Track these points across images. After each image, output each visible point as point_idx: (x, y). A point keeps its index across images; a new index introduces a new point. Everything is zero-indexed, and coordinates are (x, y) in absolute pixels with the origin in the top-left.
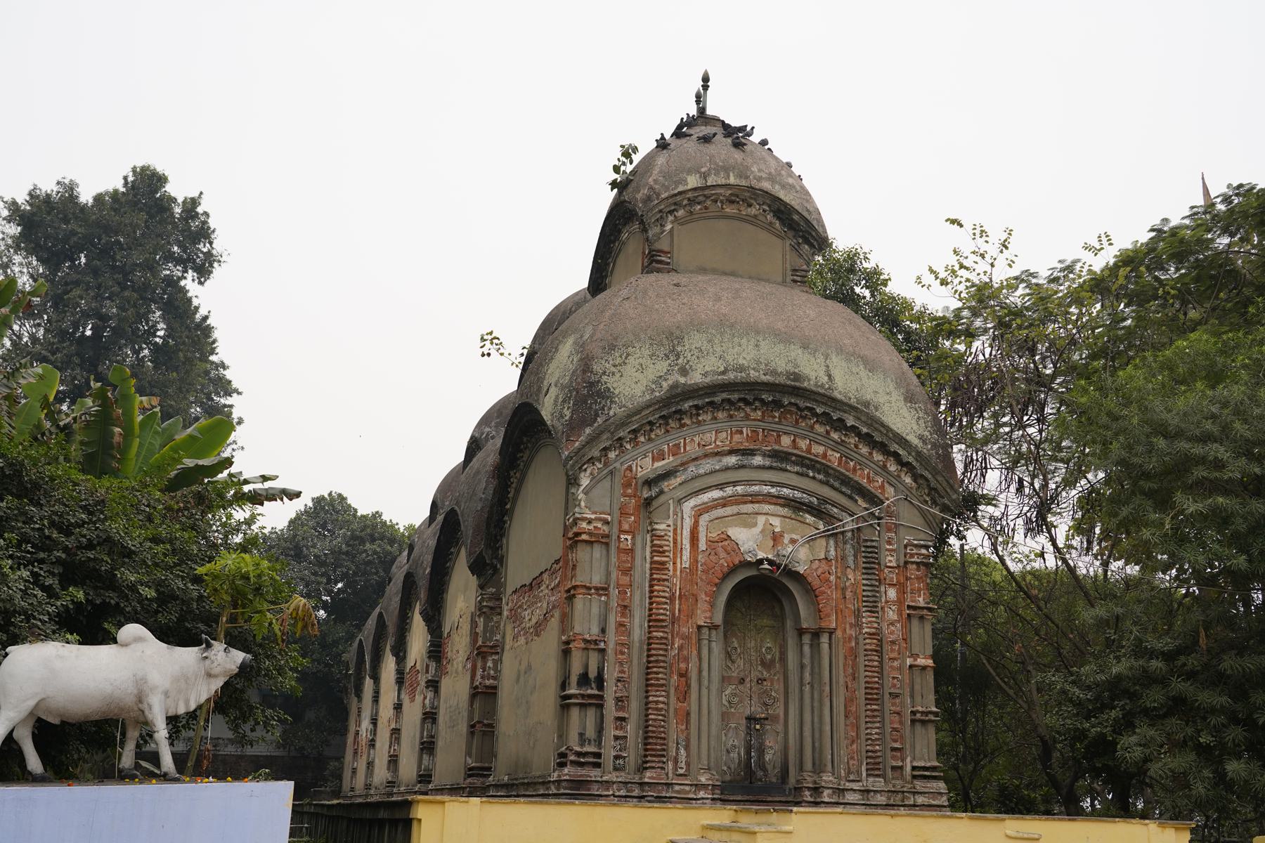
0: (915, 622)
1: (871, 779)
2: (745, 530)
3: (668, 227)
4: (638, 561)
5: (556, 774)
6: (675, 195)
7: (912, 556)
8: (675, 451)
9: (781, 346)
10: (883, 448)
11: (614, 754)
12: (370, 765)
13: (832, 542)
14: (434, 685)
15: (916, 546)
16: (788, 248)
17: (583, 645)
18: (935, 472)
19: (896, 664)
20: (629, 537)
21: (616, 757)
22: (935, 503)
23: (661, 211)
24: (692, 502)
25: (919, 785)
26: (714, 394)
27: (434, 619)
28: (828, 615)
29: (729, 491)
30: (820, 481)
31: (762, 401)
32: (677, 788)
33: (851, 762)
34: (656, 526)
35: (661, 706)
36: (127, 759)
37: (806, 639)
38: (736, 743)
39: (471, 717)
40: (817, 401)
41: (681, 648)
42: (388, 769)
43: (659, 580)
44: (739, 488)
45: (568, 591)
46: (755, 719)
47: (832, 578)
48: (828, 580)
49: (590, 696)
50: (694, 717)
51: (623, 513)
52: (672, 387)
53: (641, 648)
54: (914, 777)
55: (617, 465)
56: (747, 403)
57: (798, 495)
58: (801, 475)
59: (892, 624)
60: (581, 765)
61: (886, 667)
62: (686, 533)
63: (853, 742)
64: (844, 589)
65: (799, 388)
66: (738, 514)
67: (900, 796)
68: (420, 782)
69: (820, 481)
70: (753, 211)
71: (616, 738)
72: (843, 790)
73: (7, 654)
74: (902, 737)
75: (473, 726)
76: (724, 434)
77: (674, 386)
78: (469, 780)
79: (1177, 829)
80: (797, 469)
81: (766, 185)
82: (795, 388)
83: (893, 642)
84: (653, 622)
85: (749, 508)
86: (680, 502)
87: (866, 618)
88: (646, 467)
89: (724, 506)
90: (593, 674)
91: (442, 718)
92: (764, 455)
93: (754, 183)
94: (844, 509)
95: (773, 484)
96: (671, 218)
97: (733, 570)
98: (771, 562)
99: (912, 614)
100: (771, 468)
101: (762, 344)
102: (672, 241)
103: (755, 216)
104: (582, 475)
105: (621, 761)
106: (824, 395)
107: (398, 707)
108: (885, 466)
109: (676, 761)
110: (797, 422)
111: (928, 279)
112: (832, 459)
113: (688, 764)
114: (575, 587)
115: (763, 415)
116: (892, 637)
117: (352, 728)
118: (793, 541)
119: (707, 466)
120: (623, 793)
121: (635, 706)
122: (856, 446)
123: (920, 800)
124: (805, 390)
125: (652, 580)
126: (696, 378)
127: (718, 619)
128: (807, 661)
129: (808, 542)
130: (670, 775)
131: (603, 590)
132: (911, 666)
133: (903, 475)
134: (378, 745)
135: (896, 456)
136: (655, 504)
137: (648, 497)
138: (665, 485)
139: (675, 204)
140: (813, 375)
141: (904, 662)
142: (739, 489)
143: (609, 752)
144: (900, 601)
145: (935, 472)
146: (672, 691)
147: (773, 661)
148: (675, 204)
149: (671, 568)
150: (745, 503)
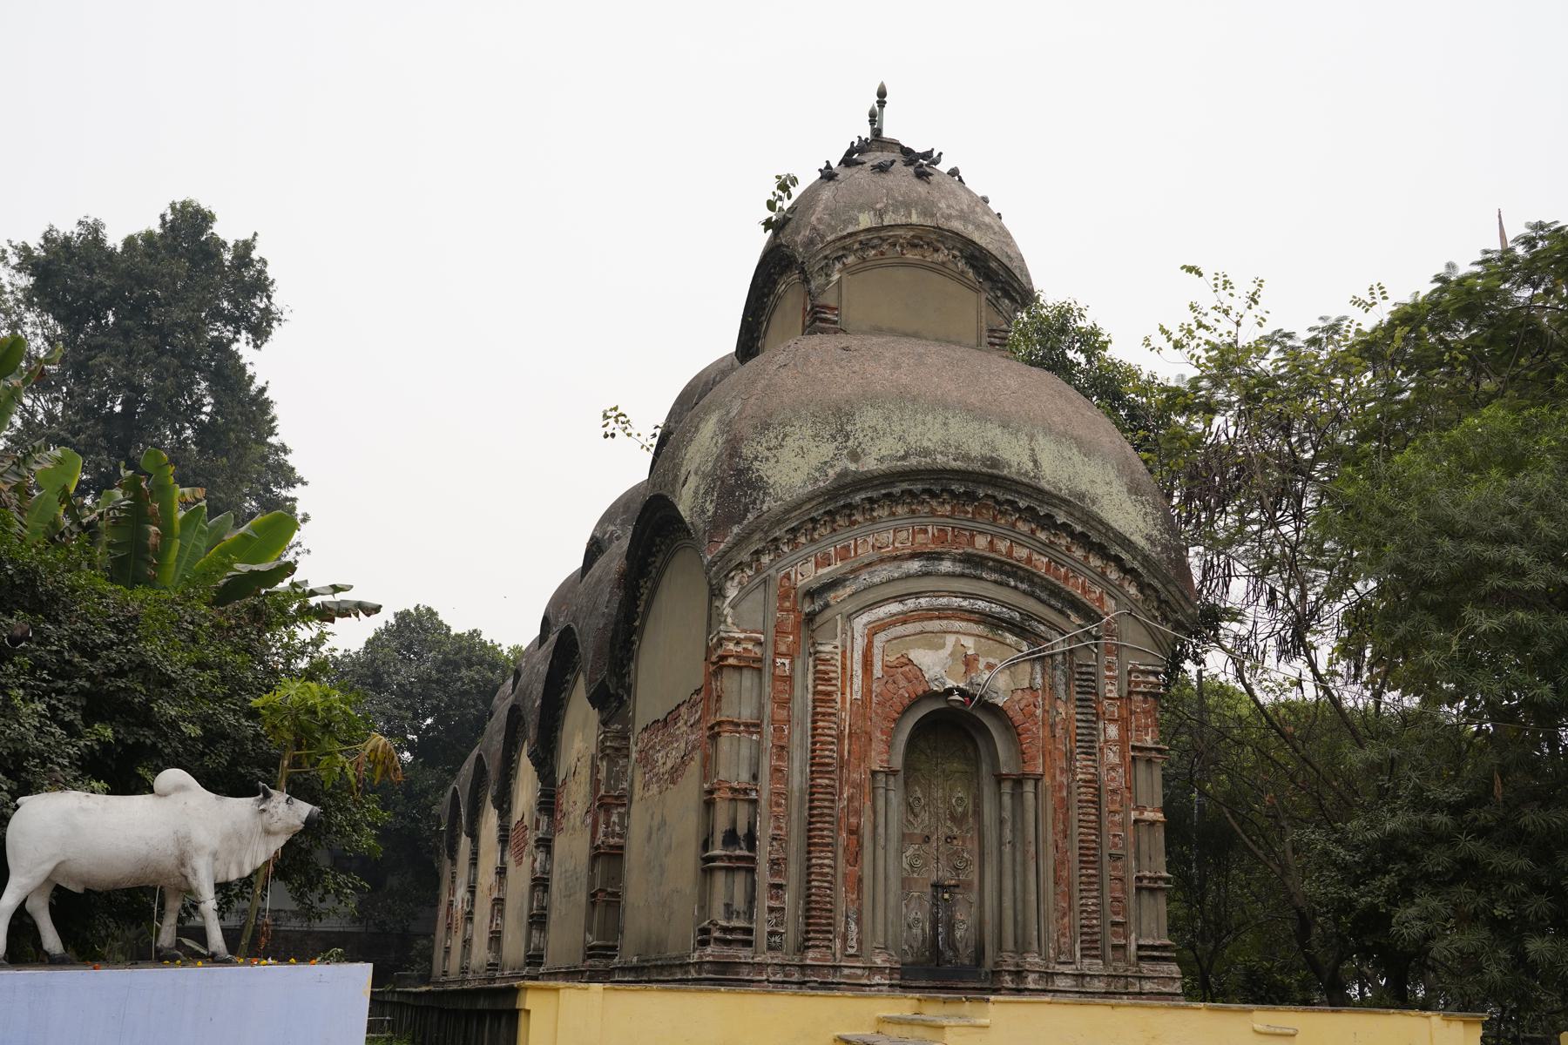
0: (1141, 767)
1: (1087, 961)
2: (930, 652)
3: (836, 277)
4: (798, 692)
5: (696, 955)
6: (844, 237)
7: (1137, 684)
8: (844, 554)
9: (976, 425)
10: (1101, 551)
12: (467, 943)
13: (1038, 668)
14: (545, 844)
15: (1142, 672)
17: (730, 795)
18: (1166, 581)
19: (1117, 818)
20: (787, 662)
21: (771, 934)
22: (1165, 618)
23: (826, 257)
24: (866, 618)
25: (1146, 968)
26: (892, 484)
27: (545, 763)
28: (1034, 758)
29: (911, 603)
30: (1024, 592)
31: (952, 492)
32: (846, 971)
33: (1062, 940)
35: (826, 870)
36: (167, 936)
37: (1007, 787)
38: (919, 915)
39: (591, 883)
40: (1019, 492)
41: (851, 799)
42: (490, 948)
43: (824, 714)
44: (922, 601)
45: (712, 728)
47: (1039, 712)
48: (1033, 715)
49: (739, 858)
50: (867, 882)
51: (780, 631)
52: (840, 476)
53: (801, 798)
54: (1140, 958)
55: (772, 572)
56: (933, 495)
57: (996, 608)
58: (1000, 584)
59: (1113, 769)
60: (728, 943)
61: (1106, 823)
62: (858, 656)
63: (1064, 915)
64: (1053, 726)
65: (997, 477)
66: (922, 632)
67: (1122, 982)
68: (528, 964)
69: (1024, 592)
70: (940, 257)
71: (771, 910)
72: (1053, 974)
73: (18, 807)
74: (1124, 908)
75: (594, 895)
76: (905, 534)
77: (844, 474)
78: (590, 962)
80: (994, 576)
81: (957, 225)
82: (992, 476)
83: (1114, 791)
84: (817, 765)
86: (849, 617)
88: (808, 574)
89: (904, 622)
90: (742, 830)
91: (556, 885)
92: (954, 560)
93: (942, 222)
94: (1052, 626)
95: (966, 596)
96: (838, 266)
97: (916, 701)
98: (962, 692)
99: (1138, 757)
100: (962, 575)
101: (952, 421)
102: (840, 295)
103: (943, 264)
104: (729, 584)
105: (777, 939)
107: (501, 872)
108: (1104, 573)
109: (845, 939)
110: (995, 517)
111: (1159, 340)
113: (860, 942)
114: (719, 724)
115: (953, 511)
116: (1113, 785)
117: (445, 898)
118: (990, 667)
119: (883, 573)
120: (779, 977)
121: (794, 869)
122: (1068, 549)
123: (1148, 986)
124: (1005, 478)
125: (815, 714)
126: (870, 464)
127: (898, 762)
128: (1007, 814)
129: (1008, 667)
130: (838, 956)
131: (754, 727)
132: (1136, 821)
133: (1126, 584)
134: (476, 918)
135: (1118, 560)
136: (819, 620)
137: (810, 612)
138: (831, 597)
140: (1014, 461)
141: (1128, 815)
142: (923, 601)
143: (762, 928)
144: (1122, 741)
145: (1166, 581)
146: (840, 851)
147: (965, 815)
149: (839, 700)
150: (931, 619)
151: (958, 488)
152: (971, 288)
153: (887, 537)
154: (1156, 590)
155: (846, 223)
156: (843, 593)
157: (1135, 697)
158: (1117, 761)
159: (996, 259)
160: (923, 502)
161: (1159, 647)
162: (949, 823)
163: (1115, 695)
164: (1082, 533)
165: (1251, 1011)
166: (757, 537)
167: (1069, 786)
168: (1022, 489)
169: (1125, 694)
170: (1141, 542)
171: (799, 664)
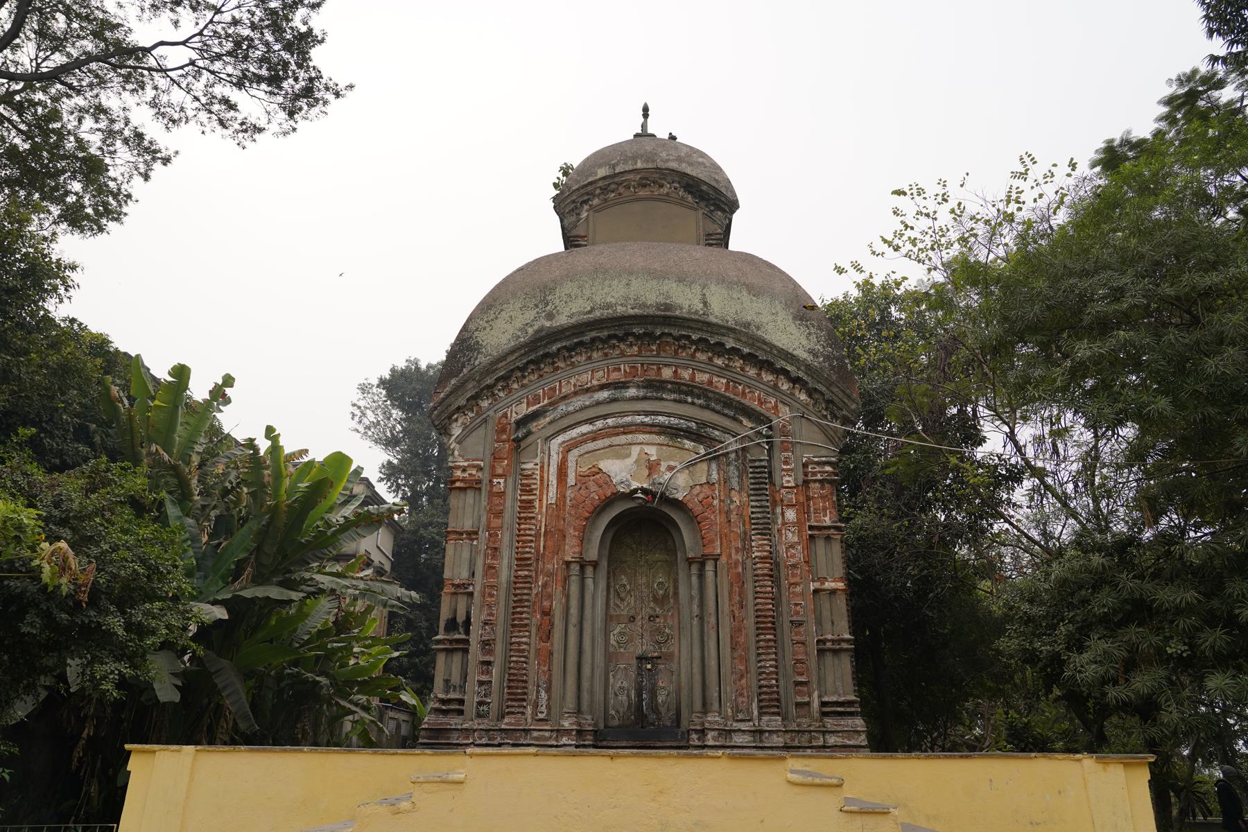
0: (820, 545)
1: (765, 718)
2: (617, 462)
3: (584, 215)
6: (586, 186)
7: (814, 474)
9: (654, 282)
11: (476, 700)
13: (714, 466)
15: (818, 463)
16: (700, 216)
18: (829, 384)
19: (798, 589)
21: (480, 703)
22: (835, 417)
23: (574, 202)
24: (560, 439)
25: (830, 723)
26: (582, 333)
28: (712, 541)
29: (599, 424)
30: (701, 406)
31: (633, 334)
32: (535, 734)
34: (524, 466)
37: (694, 569)
38: (625, 684)
40: (691, 328)
41: (545, 585)
43: (526, 518)
46: (646, 659)
47: (716, 502)
48: (711, 505)
49: (457, 641)
50: (557, 658)
51: (496, 457)
52: (537, 332)
54: (825, 714)
56: (621, 339)
57: (674, 421)
58: (680, 402)
59: (792, 546)
60: (445, 712)
61: (785, 594)
62: (553, 469)
63: (742, 676)
64: (728, 512)
65: (670, 317)
67: (806, 736)
69: (701, 406)
70: (665, 190)
71: (481, 683)
72: (730, 731)
74: (807, 669)
76: (601, 373)
79: (1125, 765)
80: (673, 396)
82: (665, 317)
83: (794, 566)
84: (522, 562)
85: (622, 439)
86: (548, 439)
87: (757, 541)
89: (594, 439)
90: (461, 618)
92: (638, 387)
93: (661, 165)
94: (726, 431)
95: (647, 414)
96: (586, 207)
97: (608, 502)
98: (644, 491)
99: (814, 535)
100: (645, 398)
101: (634, 282)
103: (667, 194)
104: (454, 425)
106: (697, 321)
110: (676, 352)
112: (719, 385)
113: (549, 707)
115: (640, 351)
116: (793, 561)
118: (670, 468)
119: (578, 402)
120: (484, 741)
122: (742, 369)
123: (832, 740)
124: (677, 318)
126: (562, 320)
127: (593, 554)
129: (687, 467)
130: (529, 720)
131: (472, 534)
132: (816, 591)
133: (797, 393)
135: (785, 372)
136: (523, 445)
137: (518, 437)
138: (533, 426)
139: (587, 194)
140: (686, 304)
142: (610, 421)
143: (471, 699)
144: (799, 523)
146: (534, 631)
147: (666, 596)
148: (587, 194)
150: (617, 434)
151: (638, 330)
152: (691, 208)
153: (586, 377)
154: (823, 394)
155: (587, 177)
156: (543, 421)
157: (812, 485)
158: (796, 539)
159: (706, 183)
160: (614, 347)
161: (831, 440)
162: (652, 604)
163: (792, 484)
164: (749, 354)
165: (784, 758)
166: (470, 386)
167: (743, 563)
168: (693, 325)
169: (800, 482)
170: (802, 354)
171: (510, 481)
